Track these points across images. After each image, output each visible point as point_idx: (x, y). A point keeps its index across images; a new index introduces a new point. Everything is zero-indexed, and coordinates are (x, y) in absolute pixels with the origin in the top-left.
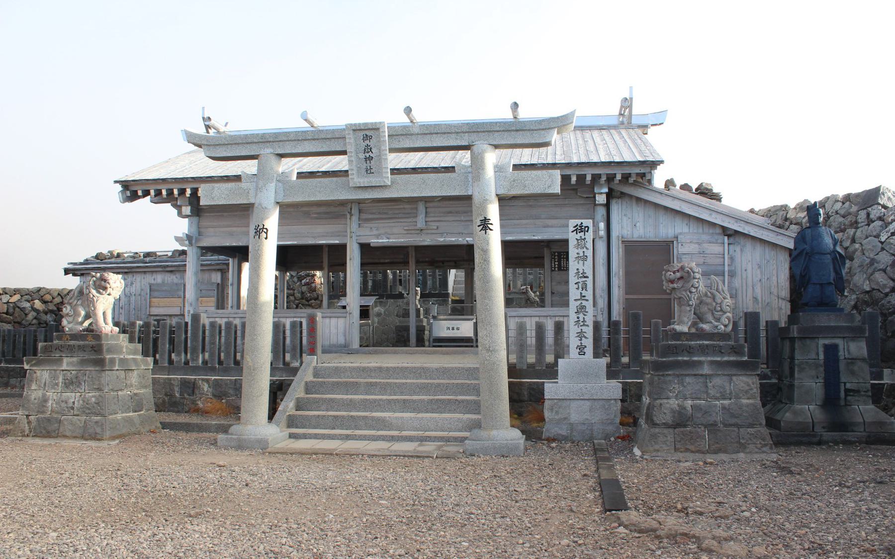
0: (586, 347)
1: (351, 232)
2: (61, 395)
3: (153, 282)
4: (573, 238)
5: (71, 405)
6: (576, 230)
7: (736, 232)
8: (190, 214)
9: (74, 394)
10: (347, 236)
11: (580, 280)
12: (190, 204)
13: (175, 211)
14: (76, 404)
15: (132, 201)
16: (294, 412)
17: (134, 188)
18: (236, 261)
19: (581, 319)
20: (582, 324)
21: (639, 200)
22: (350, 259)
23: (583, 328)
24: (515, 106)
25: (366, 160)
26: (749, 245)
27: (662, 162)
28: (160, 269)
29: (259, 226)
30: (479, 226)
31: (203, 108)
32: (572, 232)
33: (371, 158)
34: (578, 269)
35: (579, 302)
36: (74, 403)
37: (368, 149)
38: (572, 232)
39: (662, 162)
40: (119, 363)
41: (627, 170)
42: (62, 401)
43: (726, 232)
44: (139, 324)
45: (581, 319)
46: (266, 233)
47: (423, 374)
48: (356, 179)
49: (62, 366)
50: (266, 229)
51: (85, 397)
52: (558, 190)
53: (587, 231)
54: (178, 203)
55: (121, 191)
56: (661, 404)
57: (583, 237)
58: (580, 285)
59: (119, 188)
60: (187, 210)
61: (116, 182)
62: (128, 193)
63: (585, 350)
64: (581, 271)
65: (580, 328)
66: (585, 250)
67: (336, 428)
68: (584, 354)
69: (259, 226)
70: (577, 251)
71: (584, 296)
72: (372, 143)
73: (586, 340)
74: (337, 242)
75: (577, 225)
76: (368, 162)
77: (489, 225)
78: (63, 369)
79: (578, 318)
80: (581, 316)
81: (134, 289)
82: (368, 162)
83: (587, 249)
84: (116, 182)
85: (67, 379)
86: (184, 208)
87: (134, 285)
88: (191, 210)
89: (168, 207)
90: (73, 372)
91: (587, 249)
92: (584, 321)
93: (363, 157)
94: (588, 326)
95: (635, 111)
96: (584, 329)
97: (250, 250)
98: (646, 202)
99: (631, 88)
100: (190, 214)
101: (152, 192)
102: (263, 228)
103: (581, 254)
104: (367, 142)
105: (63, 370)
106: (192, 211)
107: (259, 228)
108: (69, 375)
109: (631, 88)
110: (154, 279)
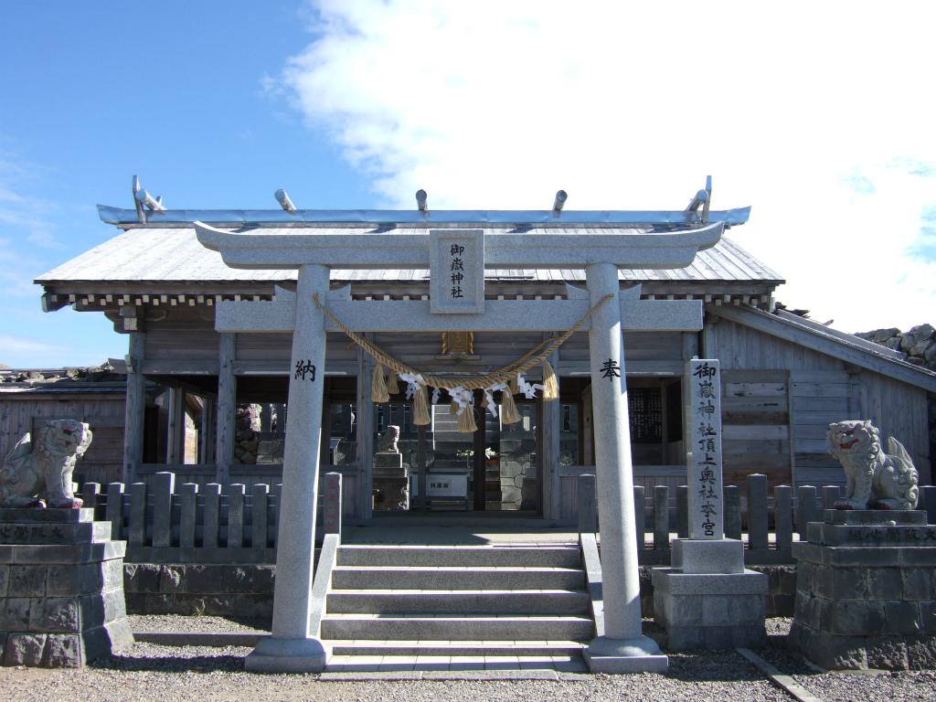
0: (714, 525)
1: (364, 361)
2: (7, 603)
3: (36, 415)
4: (693, 384)
5: (24, 616)
6: (700, 372)
7: (864, 370)
8: (136, 329)
9: (28, 600)
10: (357, 365)
11: (705, 438)
12: (138, 316)
13: (111, 324)
14: (32, 614)
15: (56, 310)
16: (325, 616)
17: (64, 292)
18: (180, 391)
19: (708, 489)
20: (708, 494)
21: (739, 326)
22: (363, 398)
23: (711, 499)
24: (562, 196)
25: (454, 280)
26: (877, 387)
27: (783, 282)
28: (50, 398)
29: (302, 362)
30: (601, 371)
31: (135, 177)
32: (695, 375)
33: (459, 277)
34: (702, 424)
35: (705, 466)
36: (28, 613)
37: (457, 264)
38: (695, 375)
39: (783, 282)
40: (94, 553)
41: (738, 290)
42: (10, 611)
43: (847, 366)
44: (924, 606)
45: (708, 489)
46: (313, 372)
47: (488, 559)
48: (440, 300)
49: (10, 558)
50: (313, 366)
51: (45, 604)
52: (700, 325)
53: (714, 374)
54: (121, 314)
55: (44, 296)
56: (846, 606)
57: (708, 382)
58: (705, 444)
59: (41, 290)
60: (131, 323)
61: (36, 282)
62: (55, 298)
63: (714, 529)
64: (706, 426)
65: (707, 500)
66: (710, 398)
67: (391, 637)
68: (712, 535)
69: (302, 362)
70: (700, 400)
71: (711, 459)
72: (463, 257)
73: (714, 516)
74: (344, 373)
75: (701, 366)
76: (456, 281)
77: (615, 370)
78: (12, 562)
79: (704, 487)
80: (707, 484)
81: (8, 424)
82: (456, 281)
83: (714, 397)
84: (36, 282)
85: (18, 578)
86: (127, 321)
87: (8, 419)
88: (138, 323)
89: (99, 317)
90: (27, 567)
91: (714, 397)
92: (711, 491)
93: (451, 274)
94: (716, 497)
95: (712, 208)
96: (712, 501)
97: (220, 381)
98: (749, 329)
99: (709, 178)
100: (136, 329)
101: (72, 298)
102: (309, 366)
103: (707, 404)
104: (457, 255)
105: (10, 565)
106: (138, 325)
107: (304, 365)
108: (20, 573)
109: (709, 178)
110: (39, 412)
